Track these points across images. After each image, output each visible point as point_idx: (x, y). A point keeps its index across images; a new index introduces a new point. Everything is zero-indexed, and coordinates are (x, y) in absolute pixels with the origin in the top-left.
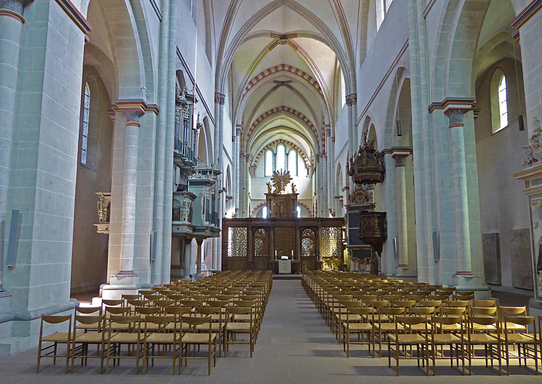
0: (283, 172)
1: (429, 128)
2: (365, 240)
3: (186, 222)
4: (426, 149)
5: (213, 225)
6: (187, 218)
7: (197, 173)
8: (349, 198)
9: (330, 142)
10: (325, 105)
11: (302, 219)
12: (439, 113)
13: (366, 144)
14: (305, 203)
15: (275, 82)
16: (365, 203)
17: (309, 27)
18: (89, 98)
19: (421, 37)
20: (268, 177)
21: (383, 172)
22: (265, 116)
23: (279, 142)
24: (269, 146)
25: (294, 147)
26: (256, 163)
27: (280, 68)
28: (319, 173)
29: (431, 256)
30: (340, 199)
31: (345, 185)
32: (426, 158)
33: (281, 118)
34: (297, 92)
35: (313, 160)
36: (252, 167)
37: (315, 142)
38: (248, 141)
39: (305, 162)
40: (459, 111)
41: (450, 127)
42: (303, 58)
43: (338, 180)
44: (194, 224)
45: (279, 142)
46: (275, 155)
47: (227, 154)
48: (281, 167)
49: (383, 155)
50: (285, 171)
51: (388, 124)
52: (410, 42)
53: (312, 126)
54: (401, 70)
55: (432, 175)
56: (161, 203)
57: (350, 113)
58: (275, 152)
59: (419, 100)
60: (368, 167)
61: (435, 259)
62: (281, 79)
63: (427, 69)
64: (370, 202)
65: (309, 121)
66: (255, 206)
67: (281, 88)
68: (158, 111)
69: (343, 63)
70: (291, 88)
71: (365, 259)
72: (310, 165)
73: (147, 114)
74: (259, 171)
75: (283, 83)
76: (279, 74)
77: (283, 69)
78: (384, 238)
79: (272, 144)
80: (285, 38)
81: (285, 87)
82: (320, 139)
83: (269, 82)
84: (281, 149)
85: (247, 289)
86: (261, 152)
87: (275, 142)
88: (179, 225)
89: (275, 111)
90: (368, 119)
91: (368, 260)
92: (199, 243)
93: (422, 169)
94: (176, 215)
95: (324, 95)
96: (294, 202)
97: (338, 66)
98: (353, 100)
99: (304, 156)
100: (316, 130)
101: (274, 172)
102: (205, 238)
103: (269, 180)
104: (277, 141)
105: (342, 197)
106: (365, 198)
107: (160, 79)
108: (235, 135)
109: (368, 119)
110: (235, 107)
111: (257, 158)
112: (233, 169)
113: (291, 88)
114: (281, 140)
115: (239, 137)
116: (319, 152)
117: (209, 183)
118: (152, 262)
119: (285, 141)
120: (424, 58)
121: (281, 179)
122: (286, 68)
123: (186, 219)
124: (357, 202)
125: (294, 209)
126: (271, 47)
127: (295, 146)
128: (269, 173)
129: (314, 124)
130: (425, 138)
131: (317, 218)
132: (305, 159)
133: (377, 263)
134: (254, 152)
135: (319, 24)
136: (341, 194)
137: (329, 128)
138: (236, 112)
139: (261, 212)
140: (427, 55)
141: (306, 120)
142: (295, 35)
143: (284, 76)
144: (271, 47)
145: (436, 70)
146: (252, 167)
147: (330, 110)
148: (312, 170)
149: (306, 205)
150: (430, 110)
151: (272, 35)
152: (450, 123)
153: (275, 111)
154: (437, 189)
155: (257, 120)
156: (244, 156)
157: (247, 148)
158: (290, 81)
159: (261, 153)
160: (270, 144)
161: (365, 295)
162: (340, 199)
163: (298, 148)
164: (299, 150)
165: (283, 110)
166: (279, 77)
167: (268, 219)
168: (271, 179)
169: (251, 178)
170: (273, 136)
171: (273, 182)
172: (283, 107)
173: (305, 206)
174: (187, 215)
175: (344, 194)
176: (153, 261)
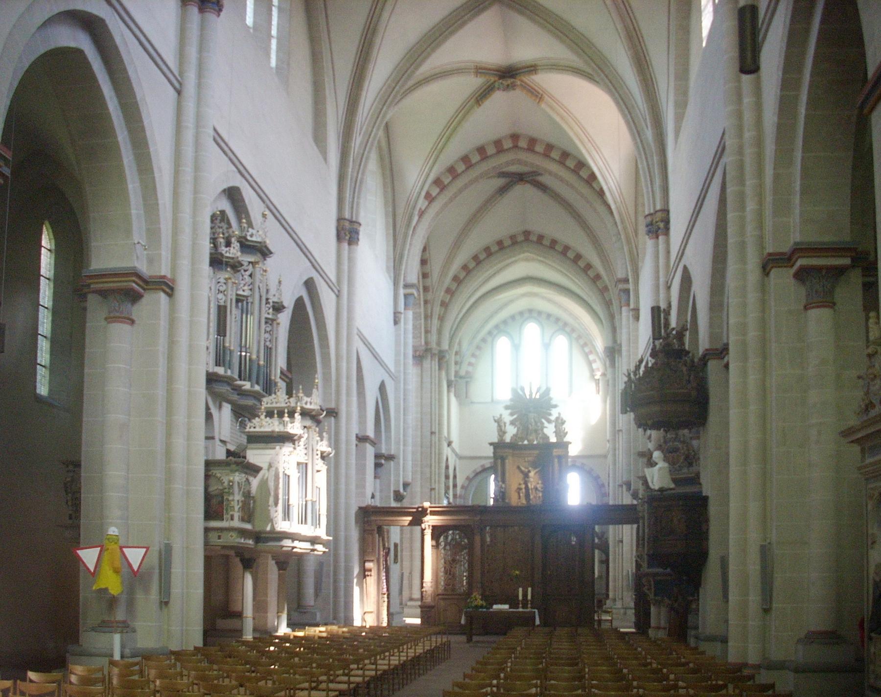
1: (763, 311)
4: (754, 361)
7: (263, 417)
12: (783, 278)
15: (503, 175)
17: (558, 51)
22: (482, 256)
27: (508, 144)
32: (753, 378)
34: (556, 197)
36: (461, 377)
38: (441, 319)
49: (705, 364)
53: (598, 277)
55: (763, 418)
64: (694, 469)
65: (589, 266)
66: (469, 473)
67: (522, 191)
68: (172, 289)
70: (543, 188)
73: (149, 298)
75: (521, 178)
77: (516, 147)
81: (528, 186)
83: (484, 175)
88: (221, 530)
89: (507, 242)
93: (744, 404)
96: (560, 463)
98: (662, 225)
101: (514, 391)
106: (687, 457)
107: (176, 220)
110: (399, 242)
111: (473, 355)
112: (397, 389)
113: (543, 188)
115: (410, 314)
121: (531, 411)
122: (523, 144)
123: (236, 516)
126: (482, 96)
129: (602, 272)
130: (752, 334)
137: (625, 286)
140: (759, 142)
143: (520, 162)
144: (482, 96)
145: (777, 177)
146: (461, 377)
147: (629, 242)
151: (480, 70)
153: (507, 242)
155: (465, 267)
166: (508, 164)
168: (507, 408)
171: (512, 414)
172: (527, 234)
174: (237, 508)
176: (167, 603)
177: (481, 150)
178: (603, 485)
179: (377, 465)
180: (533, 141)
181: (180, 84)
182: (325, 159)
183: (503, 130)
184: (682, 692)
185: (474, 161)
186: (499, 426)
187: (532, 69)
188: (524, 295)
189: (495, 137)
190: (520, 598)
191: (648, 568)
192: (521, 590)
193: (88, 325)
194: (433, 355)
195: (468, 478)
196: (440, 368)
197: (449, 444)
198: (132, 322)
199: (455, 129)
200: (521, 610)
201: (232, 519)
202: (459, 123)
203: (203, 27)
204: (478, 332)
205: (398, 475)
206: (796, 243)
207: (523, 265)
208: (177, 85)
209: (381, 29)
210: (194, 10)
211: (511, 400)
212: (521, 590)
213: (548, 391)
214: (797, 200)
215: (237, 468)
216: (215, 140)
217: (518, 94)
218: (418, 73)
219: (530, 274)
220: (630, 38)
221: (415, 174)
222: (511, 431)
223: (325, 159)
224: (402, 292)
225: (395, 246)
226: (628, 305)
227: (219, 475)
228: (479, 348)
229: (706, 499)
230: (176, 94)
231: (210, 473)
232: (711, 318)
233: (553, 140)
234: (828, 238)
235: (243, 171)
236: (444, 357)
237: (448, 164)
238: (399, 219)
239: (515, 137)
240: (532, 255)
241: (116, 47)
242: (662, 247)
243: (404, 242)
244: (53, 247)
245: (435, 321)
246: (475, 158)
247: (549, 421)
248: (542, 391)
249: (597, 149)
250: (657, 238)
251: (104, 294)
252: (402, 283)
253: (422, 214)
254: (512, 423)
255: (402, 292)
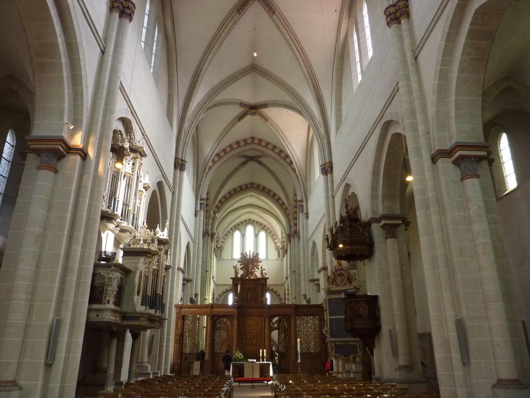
0: (251, 255)
2: (353, 332)
3: (111, 306)
4: (433, 209)
5: (152, 312)
6: (112, 300)
8: (328, 280)
9: (303, 219)
10: (297, 180)
11: (271, 306)
12: (444, 164)
13: (348, 212)
14: (275, 289)
15: (245, 156)
16: (348, 285)
17: (280, 95)
18: (14, 149)
19: (413, 78)
20: (235, 260)
21: (371, 245)
23: (248, 222)
24: (237, 226)
25: (263, 227)
26: (222, 244)
27: (250, 141)
28: (290, 255)
29: (456, 355)
30: (316, 282)
31: (321, 266)
32: (435, 218)
33: (251, 196)
35: (284, 242)
36: (218, 248)
37: (286, 222)
39: (276, 243)
40: (472, 159)
41: (462, 179)
42: (274, 130)
43: (312, 260)
44: (125, 308)
45: (248, 222)
46: (243, 236)
47: (187, 229)
48: (249, 250)
50: (254, 253)
51: (374, 189)
52: (400, 84)
53: (283, 203)
54: (388, 124)
55: (446, 242)
56: (73, 278)
57: (326, 183)
58: (243, 233)
59: (418, 150)
60: (352, 237)
61: (462, 360)
62: (250, 153)
63: (424, 111)
65: (279, 199)
67: (251, 164)
69: (317, 129)
70: (261, 163)
71: (351, 357)
72: (281, 247)
74: (225, 254)
76: (248, 147)
77: (253, 142)
78: (377, 329)
79: (240, 224)
80: (255, 109)
82: (291, 217)
84: (250, 229)
85: (212, 387)
86: (229, 232)
87: (244, 223)
88: (100, 310)
90: (348, 186)
91: (354, 358)
92: (135, 337)
94: (96, 295)
95: (296, 169)
96: (263, 288)
97: (311, 135)
98: (329, 169)
99: (274, 237)
100: (287, 208)
101: (242, 254)
102: (145, 329)
103: (236, 263)
104: (245, 221)
105: (318, 280)
106: (348, 279)
108: (199, 209)
109: (348, 186)
111: (224, 238)
112: (194, 247)
113: (261, 163)
114: (249, 220)
116: (291, 231)
117: (149, 254)
118: (49, 366)
119: (254, 221)
120: (420, 101)
121: (249, 262)
123: (111, 302)
124: (337, 285)
125: (263, 295)
127: (265, 226)
128: (237, 255)
130: (431, 194)
131: (288, 305)
132: (276, 241)
133: (370, 363)
134: (220, 231)
135: (291, 92)
136: (316, 276)
138: (200, 185)
139: (226, 299)
141: (276, 198)
142: (265, 105)
143: (254, 149)
144: (241, 117)
146: (218, 248)
147: (303, 184)
148: (283, 251)
149: (276, 291)
150: (434, 160)
151: (242, 104)
152: (462, 175)
154: (455, 260)
155: (224, 197)
156: (209, 235)
157: (212, 225)
158: (260, 157)
159: (228, 234)
160: (238, 224)
161: (342, 396)
162: (316, 282)
163: (268, 229)
164: (269, 231)
165: (252, 187)
166: (249, 150)
167: (233, 306)
168: (239, 262)
169: (217, 260)
170: (242, 215)
171: (241, 265)
172: (252, 184)
173: (276, 292)
174: (112, 296)
175: (321, 277)
177: (238, 143)
178: (281, 299)
179: (184, 284)
180: (260, 141)
181: (104, 48)
182: (172, 129)
183: (247, 135)
184: (305, 396)
185: (234, 147)
186: (236, 270)
187: (265, 105)
188: (247, 213)
189: (244, 137)
190: (261, 355)
191: (331, 337)
192: (261, 350)
193: (24, 172)
194: (209, 235)
195: (219, 295)
196: (212, 241)
197: (213, 277)
198: (56, 171)
199: (224, 136)
200: (265, 362)
201: (108, 302)
202: (230, 129)
203: (120, 25)
204: (226, 228)
205: (192, 290)
206: (457, 142)
207: (248, 199)
208: (103, 48)
209: (202, 73)
210: (117, 15)
211: (241, 258)
212: (261, 350)
213: (257, 254)
214: (453, 121)
215: (115, 269)
216: (120, 88)
217: (257, 117)
218: (215, 100)
219: (251, 203)
220: (314, 88)
221: (208, 149)
222: (241, 273)
223: (172, 129)
224: (199, 202)
225: (197, 182)
226: (303, 212)
227: (102, 273)
228: (226, 235)
229: (376, 298)
230: (101, 53)
231: (97, 272)
232: (372, 203)
233: (269, 140)
234: (472, 141)
235: (133, 112)
236: (214, 236)
237: (223, 147)
238: (200, 169)
239: (253, 138)
240: (254, 194)
241: (68, 4)
242: (329, 179)
243: (202, 179)
244: (15, 144)
245: (211, 220)
246: (235, 146)
247: (258, 269)
248: (255, 255)
249: (290, 144)
250: (327, 175)
251: (38, 152)
252: (199, 198)
253: (210, 168)
254: (241, 269)
255: (199, 202)
